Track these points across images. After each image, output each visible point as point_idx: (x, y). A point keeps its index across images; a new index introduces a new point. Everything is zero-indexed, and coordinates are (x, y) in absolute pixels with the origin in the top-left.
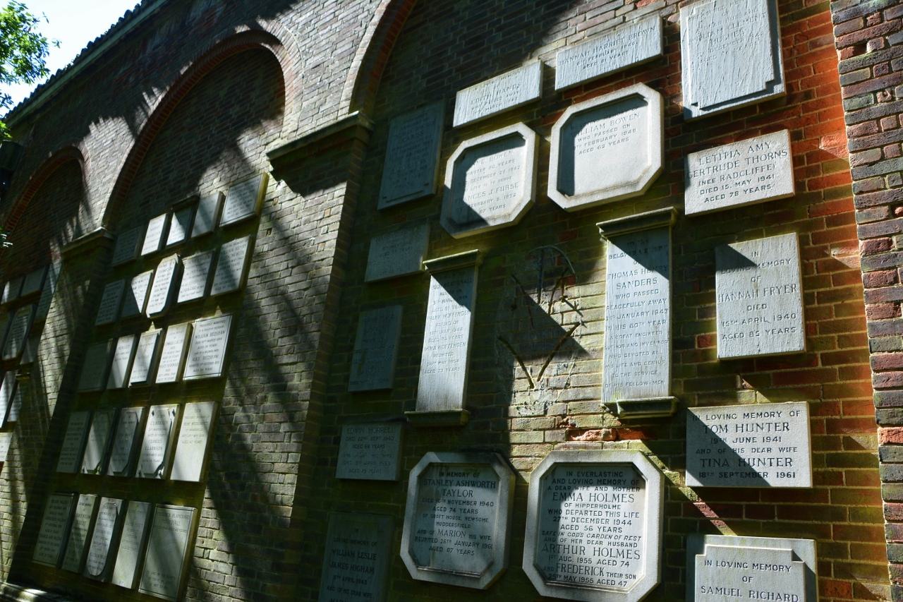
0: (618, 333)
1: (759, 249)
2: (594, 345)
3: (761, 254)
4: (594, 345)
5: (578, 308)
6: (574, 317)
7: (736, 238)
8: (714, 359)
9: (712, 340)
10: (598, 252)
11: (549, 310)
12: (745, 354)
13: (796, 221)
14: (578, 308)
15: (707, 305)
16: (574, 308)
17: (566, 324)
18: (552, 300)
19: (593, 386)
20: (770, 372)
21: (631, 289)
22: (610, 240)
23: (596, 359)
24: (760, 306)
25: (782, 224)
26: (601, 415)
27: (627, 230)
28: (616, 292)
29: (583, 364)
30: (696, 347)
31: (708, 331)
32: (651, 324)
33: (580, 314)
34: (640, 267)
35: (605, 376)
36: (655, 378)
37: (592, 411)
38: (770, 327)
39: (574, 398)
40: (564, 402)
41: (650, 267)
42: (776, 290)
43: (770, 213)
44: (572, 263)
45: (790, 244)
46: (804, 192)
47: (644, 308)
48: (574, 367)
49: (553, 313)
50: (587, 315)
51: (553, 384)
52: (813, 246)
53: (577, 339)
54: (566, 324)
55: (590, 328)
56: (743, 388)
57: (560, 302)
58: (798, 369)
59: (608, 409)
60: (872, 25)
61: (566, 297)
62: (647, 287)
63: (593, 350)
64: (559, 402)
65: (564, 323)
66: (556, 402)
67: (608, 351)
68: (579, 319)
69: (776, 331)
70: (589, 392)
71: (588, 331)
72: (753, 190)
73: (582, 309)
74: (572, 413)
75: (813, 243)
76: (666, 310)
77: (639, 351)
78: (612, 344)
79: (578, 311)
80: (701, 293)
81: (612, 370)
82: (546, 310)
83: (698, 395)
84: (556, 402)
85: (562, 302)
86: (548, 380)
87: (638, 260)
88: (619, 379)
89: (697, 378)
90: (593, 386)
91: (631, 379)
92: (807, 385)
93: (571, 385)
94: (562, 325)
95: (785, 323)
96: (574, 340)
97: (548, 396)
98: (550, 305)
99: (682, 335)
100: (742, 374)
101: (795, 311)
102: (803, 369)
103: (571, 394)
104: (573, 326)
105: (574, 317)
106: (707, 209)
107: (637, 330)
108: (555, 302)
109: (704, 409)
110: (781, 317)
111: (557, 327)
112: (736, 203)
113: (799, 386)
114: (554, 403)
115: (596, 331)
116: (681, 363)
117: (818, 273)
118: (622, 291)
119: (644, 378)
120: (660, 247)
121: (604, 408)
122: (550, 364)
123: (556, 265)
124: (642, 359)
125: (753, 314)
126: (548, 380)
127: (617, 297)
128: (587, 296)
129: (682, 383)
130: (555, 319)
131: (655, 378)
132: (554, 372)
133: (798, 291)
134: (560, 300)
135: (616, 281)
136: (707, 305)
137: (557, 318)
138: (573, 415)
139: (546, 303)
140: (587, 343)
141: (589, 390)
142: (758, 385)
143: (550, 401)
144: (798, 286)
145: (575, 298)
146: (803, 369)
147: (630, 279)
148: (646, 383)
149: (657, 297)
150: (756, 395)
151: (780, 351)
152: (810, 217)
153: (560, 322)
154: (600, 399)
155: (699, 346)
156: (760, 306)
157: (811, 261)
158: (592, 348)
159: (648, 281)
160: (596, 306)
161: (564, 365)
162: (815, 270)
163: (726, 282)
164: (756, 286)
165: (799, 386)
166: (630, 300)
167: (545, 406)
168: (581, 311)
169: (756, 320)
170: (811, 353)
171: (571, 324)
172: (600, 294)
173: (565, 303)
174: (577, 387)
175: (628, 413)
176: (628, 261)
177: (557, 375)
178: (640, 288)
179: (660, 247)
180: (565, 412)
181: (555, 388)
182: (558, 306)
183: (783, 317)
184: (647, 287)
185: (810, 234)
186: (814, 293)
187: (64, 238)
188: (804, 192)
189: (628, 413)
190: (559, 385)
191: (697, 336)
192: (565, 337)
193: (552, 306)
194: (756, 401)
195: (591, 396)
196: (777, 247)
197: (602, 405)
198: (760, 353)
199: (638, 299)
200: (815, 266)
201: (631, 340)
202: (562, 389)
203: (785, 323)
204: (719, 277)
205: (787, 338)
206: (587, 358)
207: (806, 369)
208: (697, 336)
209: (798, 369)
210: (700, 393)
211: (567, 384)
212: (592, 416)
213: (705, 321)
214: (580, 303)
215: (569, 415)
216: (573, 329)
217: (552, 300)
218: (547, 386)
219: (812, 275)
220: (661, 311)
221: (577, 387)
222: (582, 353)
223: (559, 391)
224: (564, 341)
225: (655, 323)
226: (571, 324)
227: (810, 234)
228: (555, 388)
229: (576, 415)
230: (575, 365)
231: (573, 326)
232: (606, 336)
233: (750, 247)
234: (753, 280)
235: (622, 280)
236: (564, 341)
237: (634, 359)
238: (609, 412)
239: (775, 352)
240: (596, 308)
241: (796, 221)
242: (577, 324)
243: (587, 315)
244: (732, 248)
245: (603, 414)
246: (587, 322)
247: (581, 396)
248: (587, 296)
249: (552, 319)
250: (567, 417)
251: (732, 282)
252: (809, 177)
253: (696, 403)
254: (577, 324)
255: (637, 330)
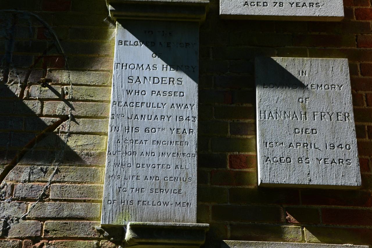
0: (128, 136)
1: (307, 69)
2: (88, 147)
3: (309, 74)
4: (88, 147)
5: (67, 97)
6: (60, 107)
7: (276, 53)
8: (251, 184)
9: (252, 162)
10: (102, 34)
11: (22, 93)
12: (293, 182)
13: (342, 48)
14: (67, 97)
15: (241, 121)
16: (61, 97)
17: (47, 116)
18: (26, 81)
19: (85, 201)
20: (319, 207)
21: (148, 86)
22: (120, 22)
23: (90, 166)
24: (309, 131)
25: (329, 48)
26: (95, 242)
27: (146, 15)
28: (127, 86)
29: (71, 173)
30: (228, 167)
31: (242, 151)
32: (174, 132)
33: (70, 106)
34: (160, 62)
35: (107, 188)
36: (178, 198)
37: (82, 235)
38: (321, 155)
39: (53, 215)
40: (37, 219)
41: (175, 65)
42: (327, 116)
43: (314, 33)
44: (60, 40)
45: (342, 70)
46: (352, 20)
47: (165, 111)
48: (56, 173)
49: (26, 99)
50: (80, 109)
51: (20, 193)
52: (362, 77)
53: (63, 137)
54: (47, 116)
55: (83, 125)
56: (288, 222)
57: (39, 86)
58: (351, 208)
59: (106, 234)
60: (155, 83)
61: (50, 81)
62: (169, 88)
63: (87, 154)
64: (29, 219)
65: (44, 113)
66: (24, 218)
67: (113, 158)
68: (68, 111)
69: (329, 161)
70: (78, 209)
71: (81, 128)
72: (301, 5)
73: (73, 100)
74: (50, 235)
75: (362, 74)
76: (194, 117)
77: (156, 163)
78: (120, 149)
79: (67, 102)
80: (232, 105)
81: (117, 183)
82: (18, 93)
83: (231, 225)
84: (24, 218)
85: (43, 86)
86: (13, 186)
87: (158, 53)
88: (128, 195)
89: (229, 204)
90: (85, 201)
91: (145, 196)
92: (361, 226)
93: (50, 197)
94: (41, 115)
95: (339, 153)
96: (59, 138)
97: (12, 209)
98: (23, 87)
99: (210, 151)
100: (285, 206)
101: (349, 141)
102: (356, 208)
103: (49, 209)
104: (58, 119)
105: (60, 107)
106: (246, 14)
107: (154, 136)
108: (31, 84)
109: (244, 244)
110: (334, 146)
111: (35, 119)
112: (281, 14)
113: (353, 227)
114: (20, 220)
115: (91, 131)
116: (209, 184)
117: (368, 105)
118: (135, 86)
119: (163, 197)
120: (187, 44)
121: (100, 232)
122: (18, 166)
123: (36, 37)
124: (161, 173)
125: (303, 138)
126: (13, 186)
127: (129, 92)
128: (82, 85)
129: (210, 208)
130: (30, 106)
131: (178, 198)
132: (24, 176)
133: (352, 121)
134: (39, 83)
135: (127, 72)
136: (241, 121)
137: (34, 106)
138: (51, 239)
139: (16, 83)
140: (79, 144)
141: (79, 206)
142: (305, 221)
143: (14, 216)
144: (352, 115)
145: (64, 85)
146: (356, 208)
147: (147, 73)
148: (166, 204)
149: (183, 100)
150: (303, 232)
151: (334, 183)
152: (358, 47)
153: (38, 112)
154: (98, 219)
155: (231, 166)
156: (309, 131)
157: (360, 92)
158: (85, 151)
159: (171, 80)
160: (93, 99)
161: (42, 169)
162: (365, 102)
163: (269, 97)
164: (304, 108)
165: (353, 227)
166: (146, 98)
167: (6, 224)
168: (71, 103)
169: (305, 145)
170: (365, 190)
171: (55, 116)
172: (100, 86)
173: (47, 88)
174: (60, 200)
175: (143, 241)
176: (144, 54)
177: (29, 181)
178: (159, 87)
179: (187, 44)
180: (39, 234)
181: (25, 199)
182: (35, 90)
183: (336, 146)
184: (169, 88)
185: (358, 64)
186: (364, 126)
187: (34, 199)
188: (352, 20)
189: (143, 241)
190: (32, 195)
191: (229, 154)
192: (43, 132)
193: (27, 89)
194: (303, 240)
195: (82, 214)
196: (327, 70)
197: (99, 227)
198: (311, 183)
199: (155, 99)
200: (364, 97)
201: (145, 147)
202: (35, 201)
203: (339, 153)
204: (259, 92)
205: (342, 170)
206: (77, 163)
207: (360, 208)
208: (229, 154)
209: (351, 208)
210: (232, 222)
211: (44, 194)
212: (82, 242)
213: (239, 139)
214: (71, 92)
215: (45, 238)
216: (58, 123)
217: (26, 81)
218: (11, 195)
219: (361, 107)
220: (188, 119)
221: (60, 200)
222: (72, 158)
223: (30, 205)
224: (43, 136)
225: (180, 131)
226: (55, 116)
227: (358, 64)
228: (25, 199)
229: (56, 239)
230: (58, 171)
231: (58, 119)
232: (111, 139)
233: (297, 64)
234: (300, 100)
235: (135, 73)
236: (43, 136)
237: (150, 172)
238: (108, 238)
239: (329, 184)
240: (92, 101)
241: (342, 48)
242: (64, 118)
243: (80, 109)
244: (275, 62)
245: (99, 239)
246: (79, 117)
247: (65, 214)
248: (82, 85)
249: (26, 106)
250: (42, 242)
251: (276, 98)
252: (357, 5)
253: (229, 235)
254: (64, 118)
255: (154, 136)
